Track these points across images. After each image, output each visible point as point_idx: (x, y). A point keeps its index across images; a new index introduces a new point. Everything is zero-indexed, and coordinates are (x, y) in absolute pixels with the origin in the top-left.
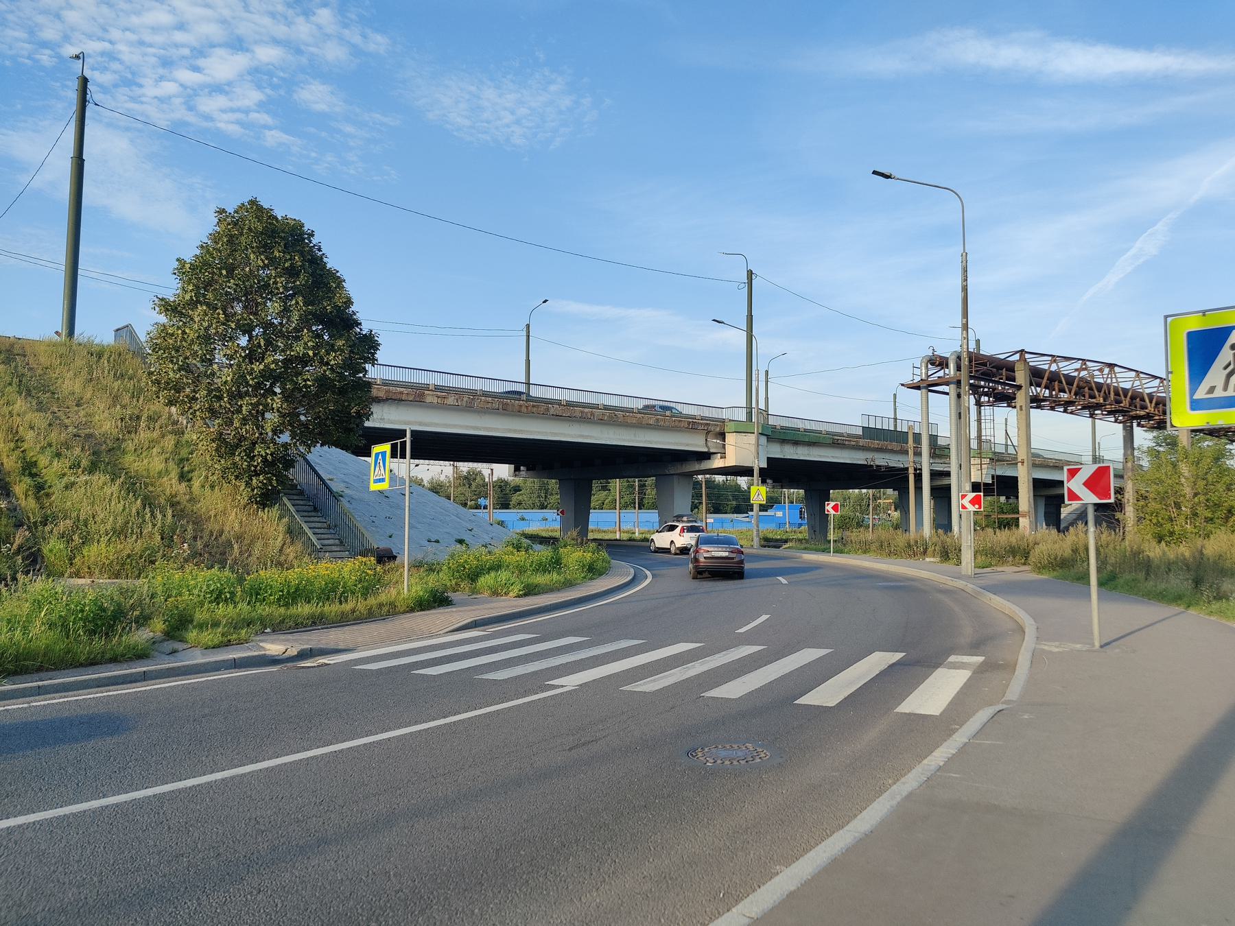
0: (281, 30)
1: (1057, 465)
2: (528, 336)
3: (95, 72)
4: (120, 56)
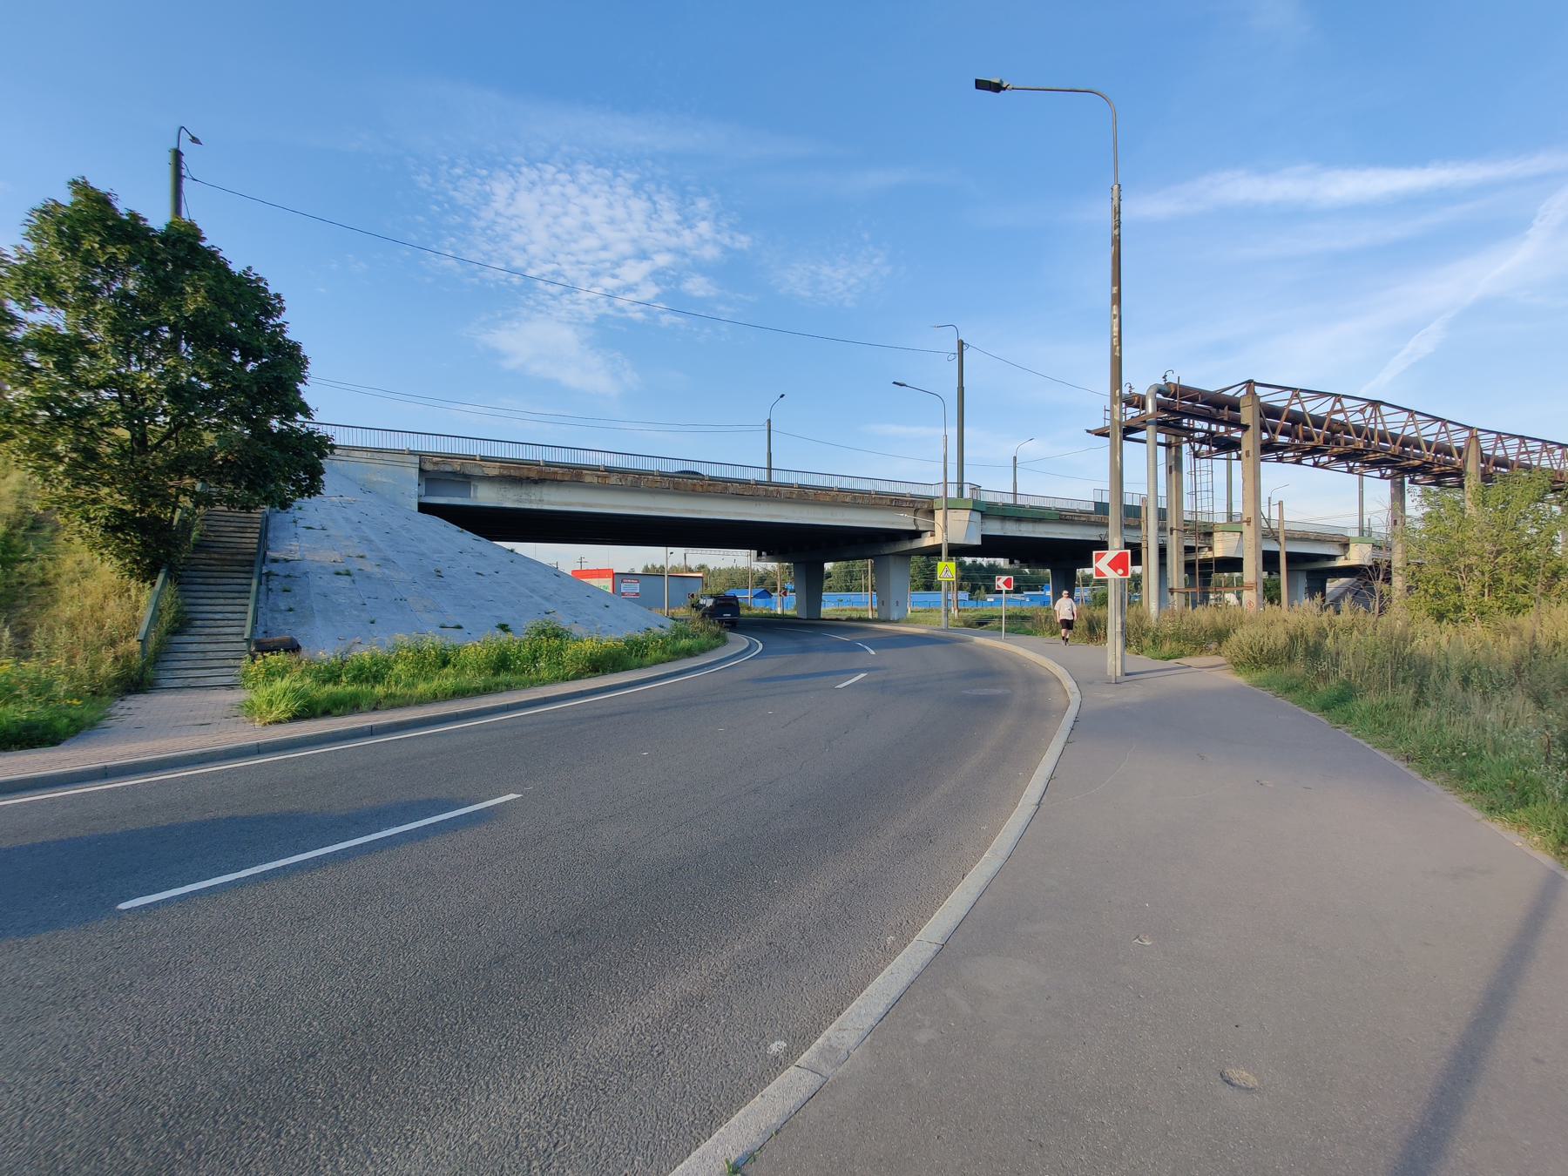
0: (673, 241)
1: (1319, 538)
2: (770, 431)
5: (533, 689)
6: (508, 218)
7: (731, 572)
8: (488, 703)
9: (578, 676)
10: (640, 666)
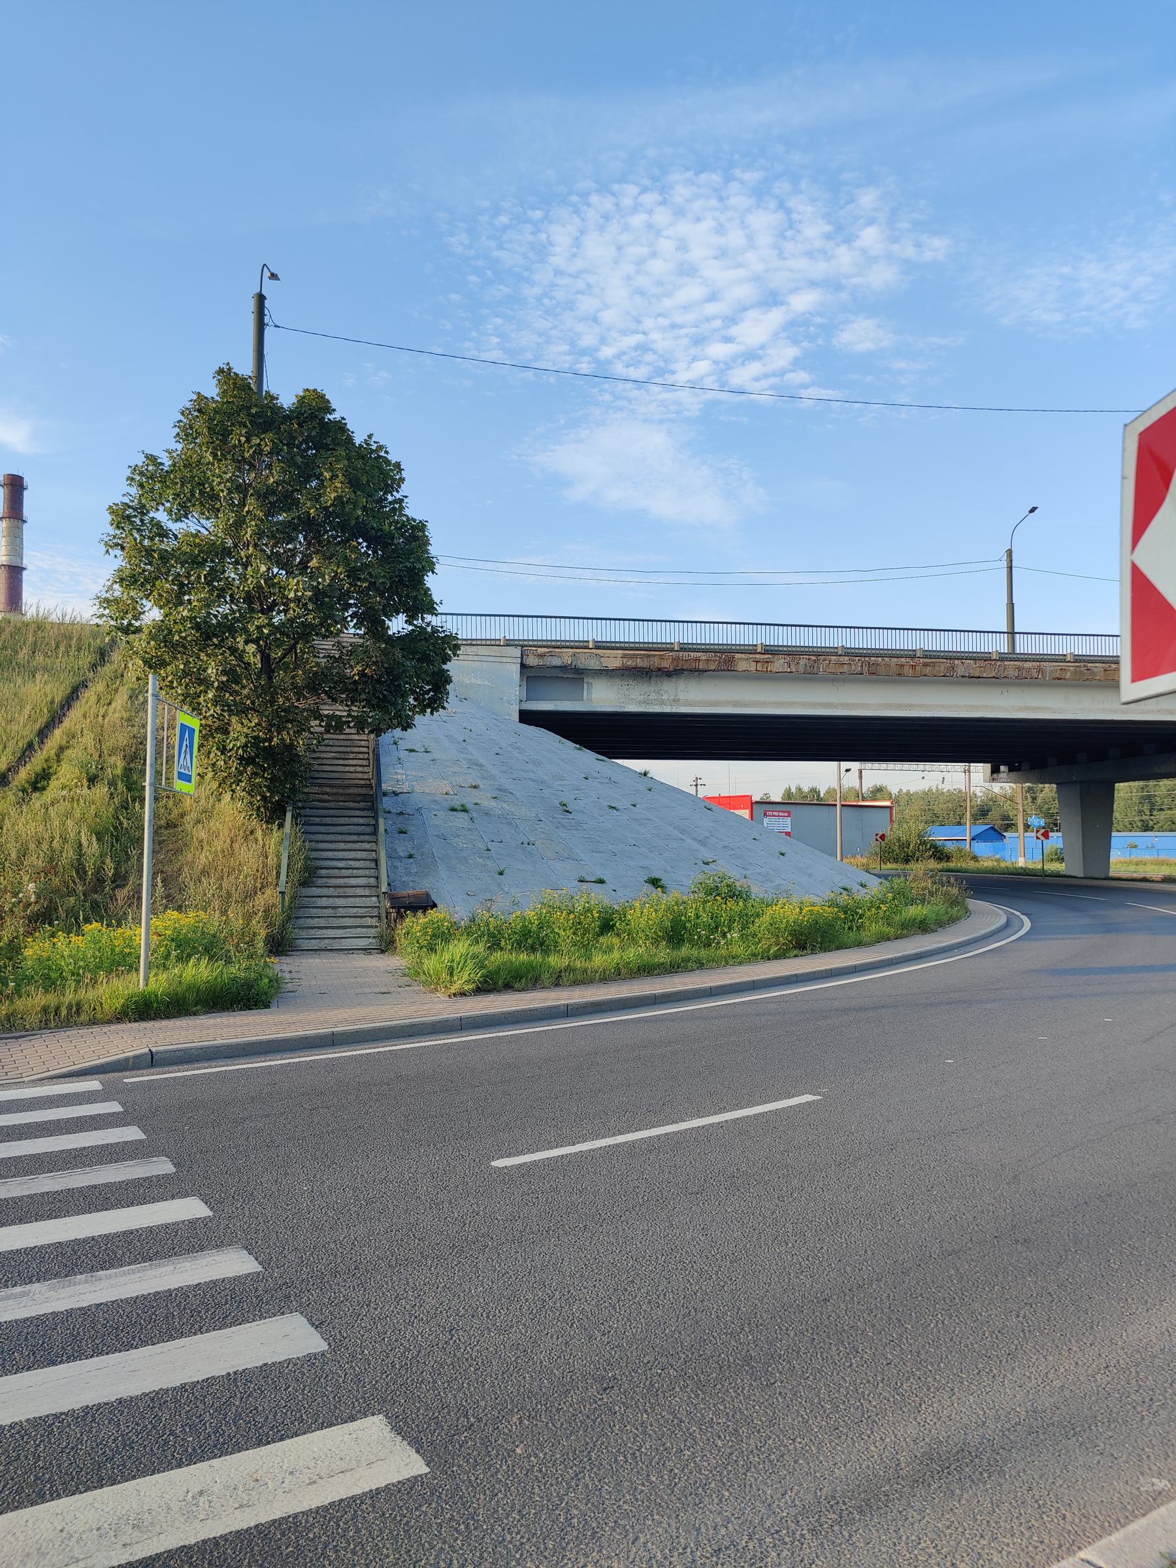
0: (820, 268)
2: (1010, 568)
3: (630, 368)
4: (655, 346)
5: (729, 969)
6: (570, 275)
7: (929, 797)
8: (684, 984)
9: (780, 956)
10: (860, 944)
